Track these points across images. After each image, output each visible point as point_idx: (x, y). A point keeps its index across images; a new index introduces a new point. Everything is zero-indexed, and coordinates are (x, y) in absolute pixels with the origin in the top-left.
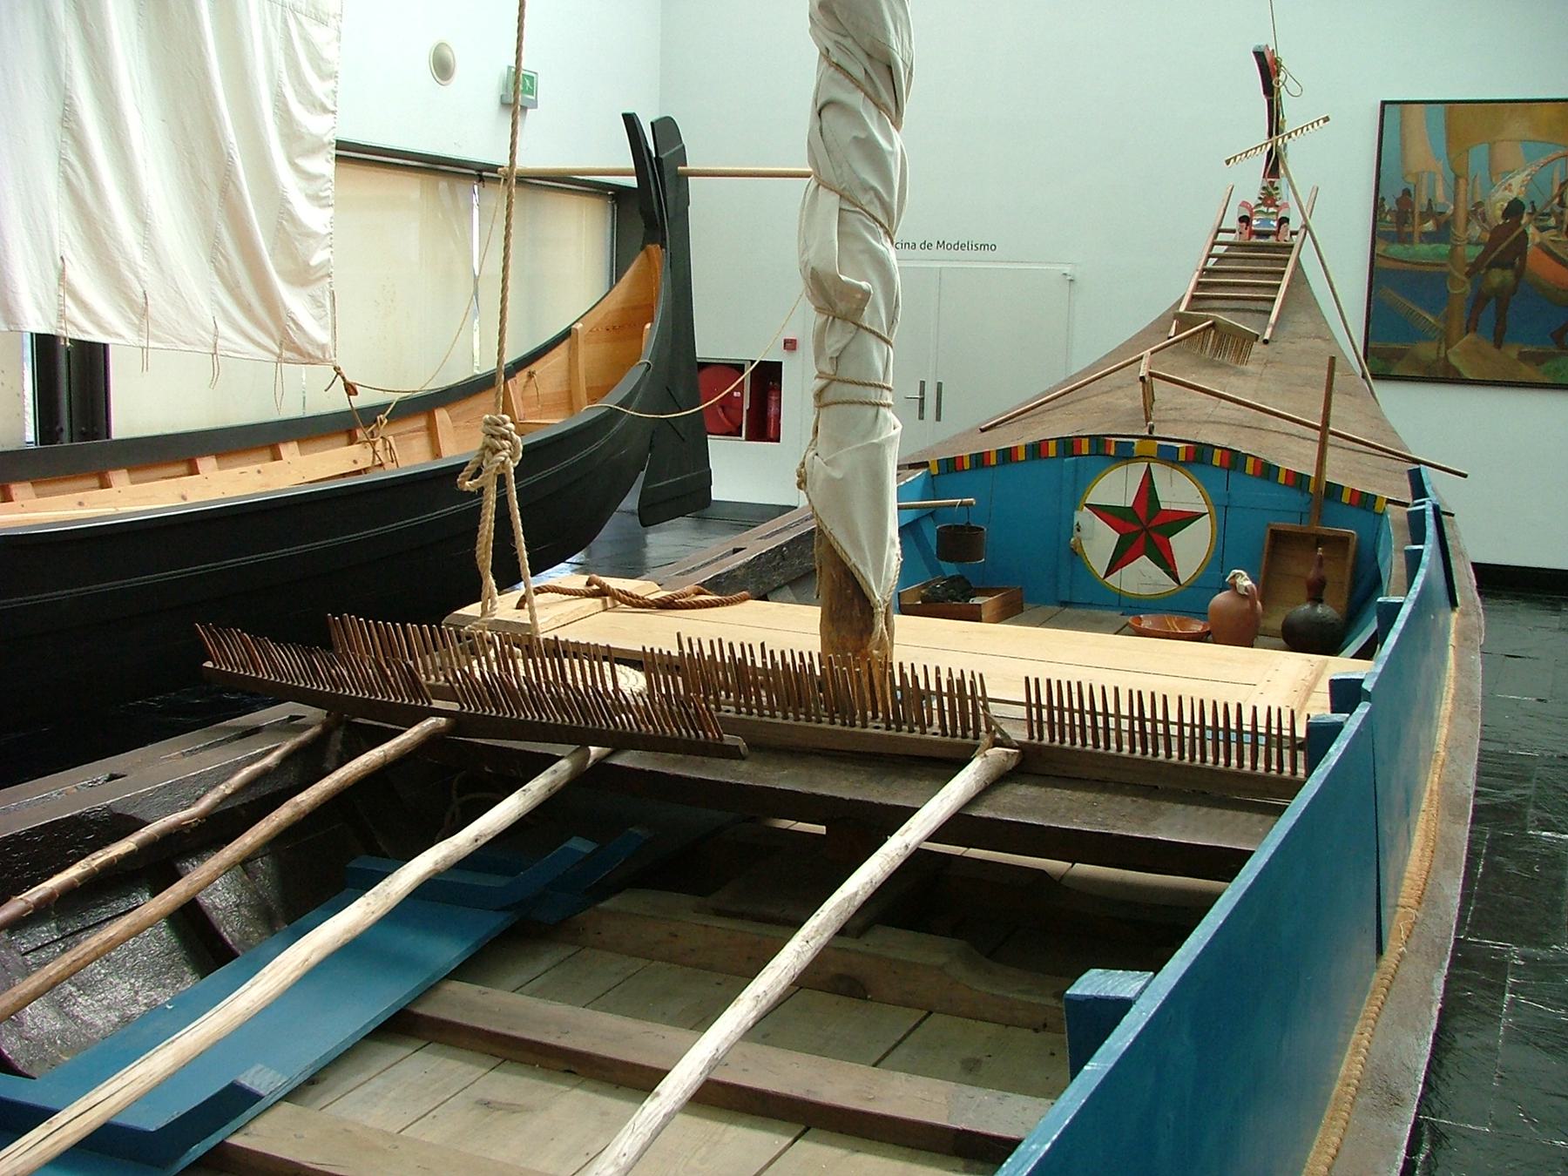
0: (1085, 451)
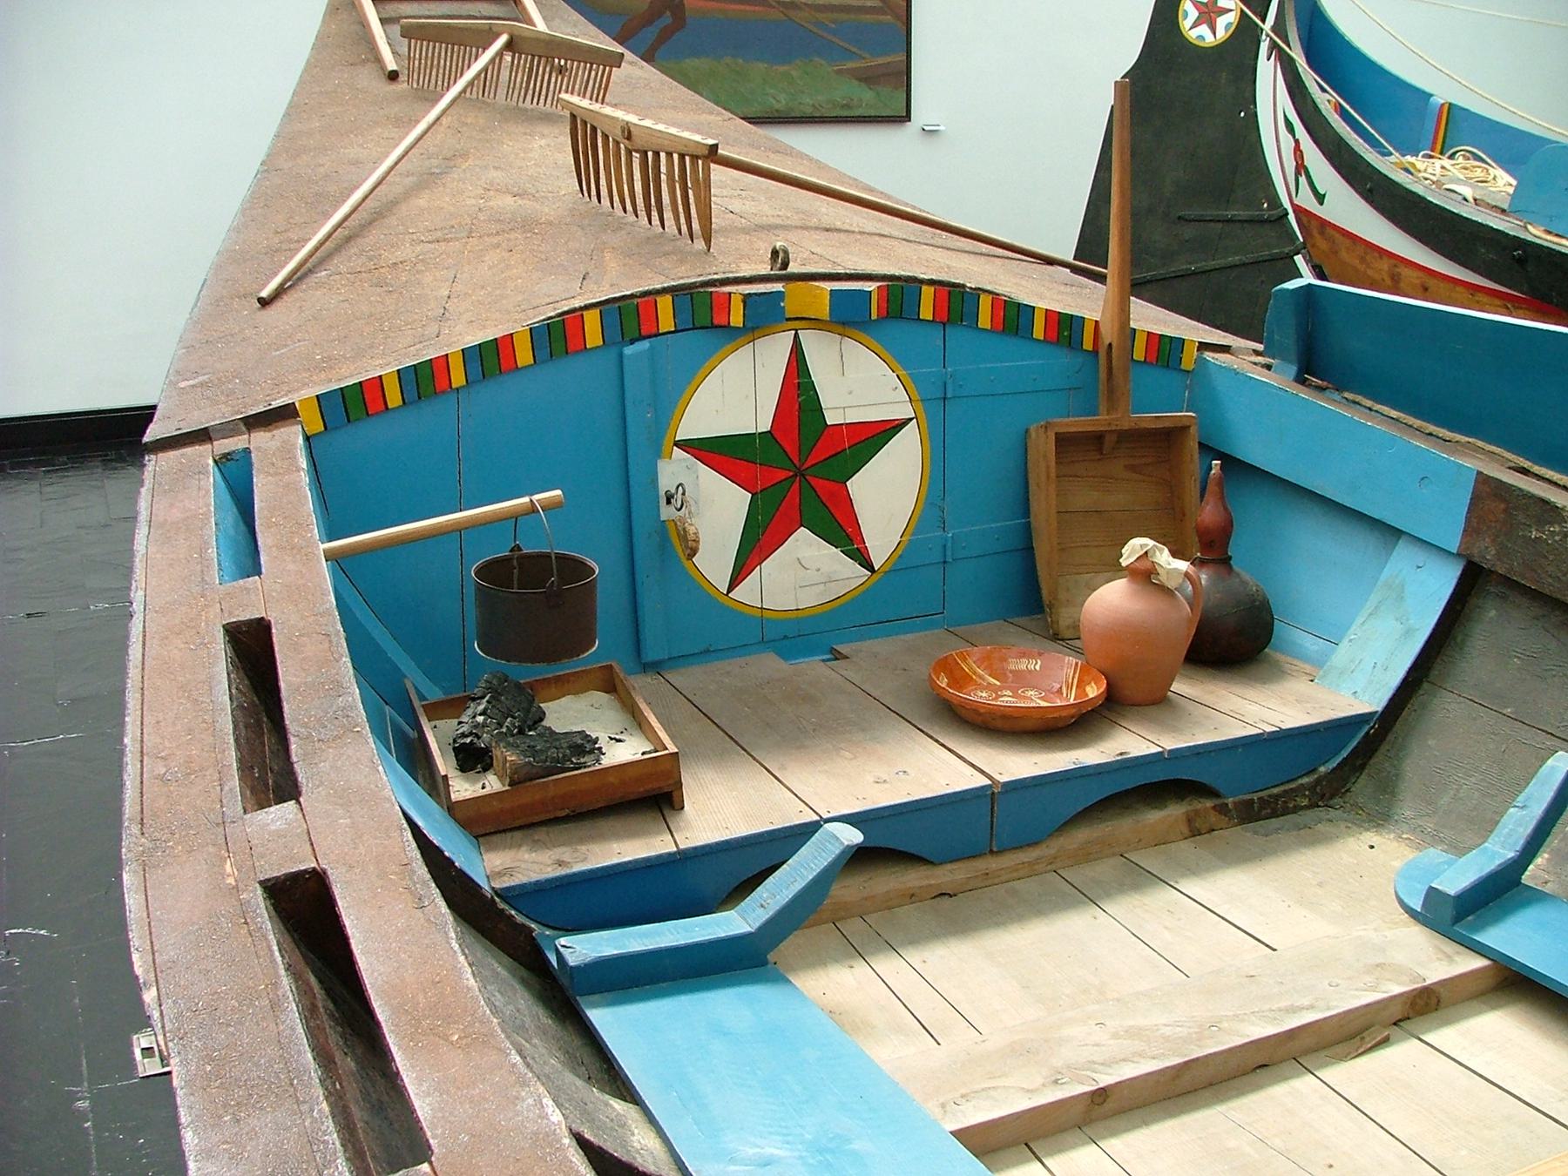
0: (666, 322)
